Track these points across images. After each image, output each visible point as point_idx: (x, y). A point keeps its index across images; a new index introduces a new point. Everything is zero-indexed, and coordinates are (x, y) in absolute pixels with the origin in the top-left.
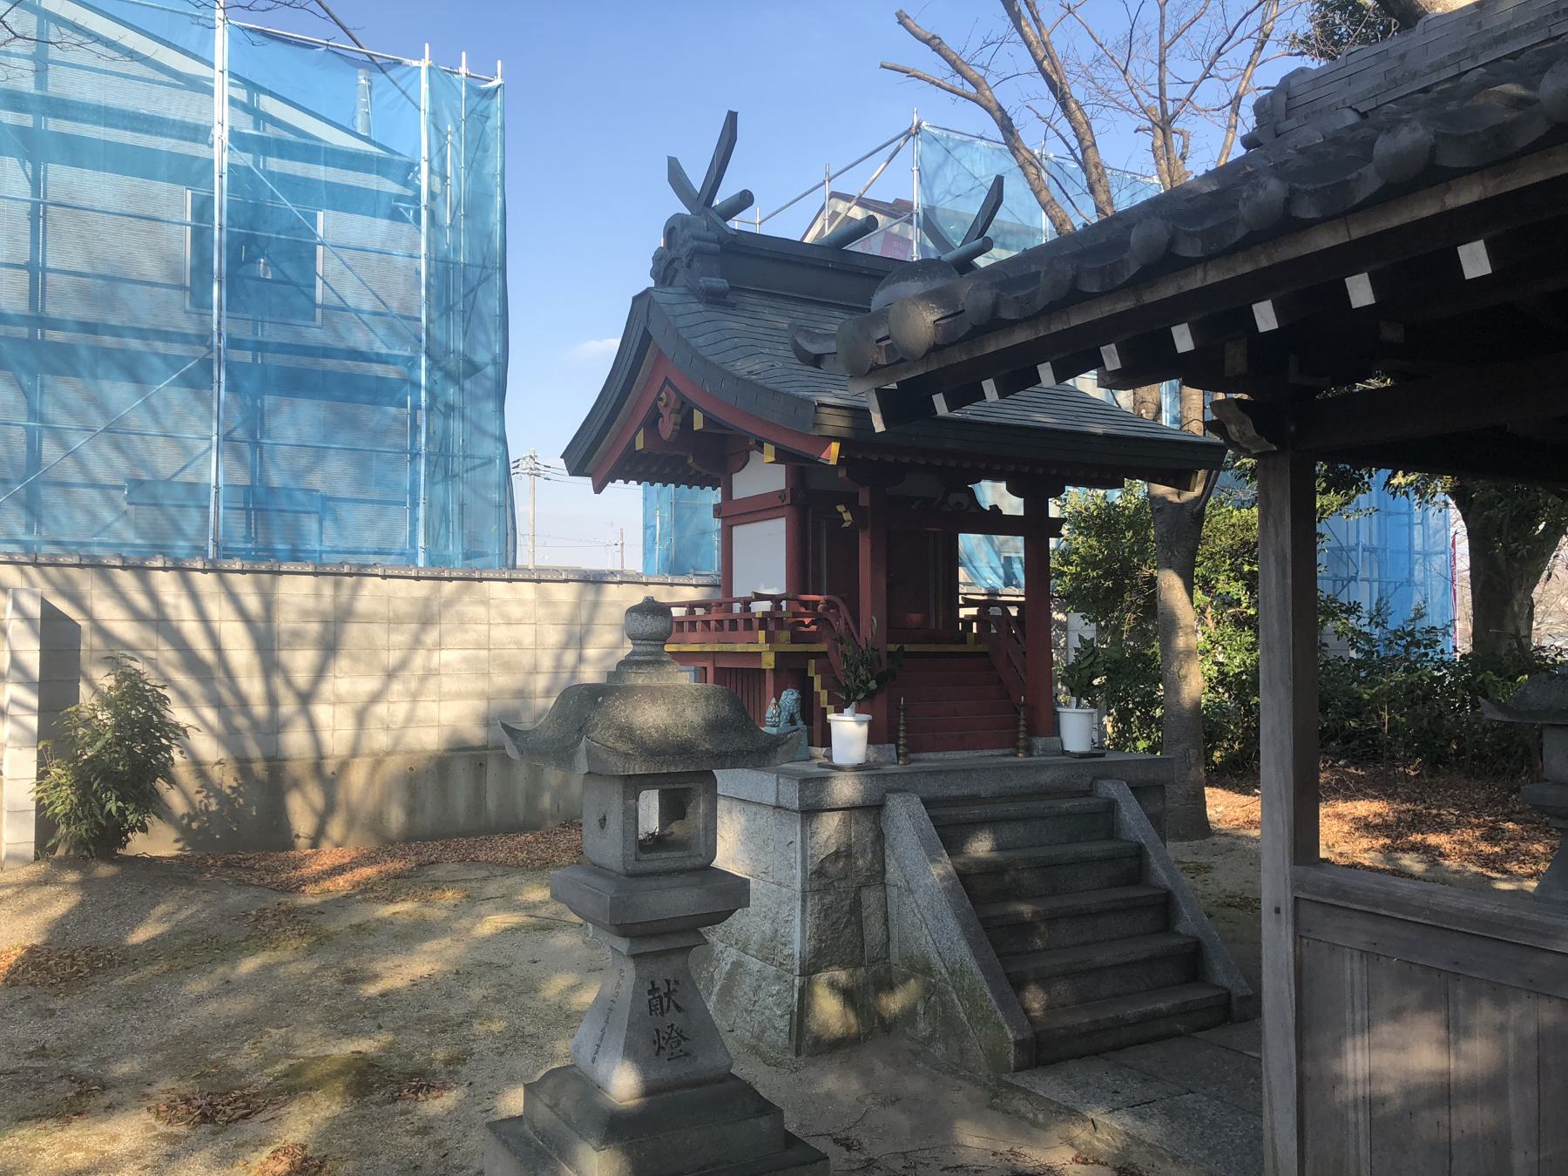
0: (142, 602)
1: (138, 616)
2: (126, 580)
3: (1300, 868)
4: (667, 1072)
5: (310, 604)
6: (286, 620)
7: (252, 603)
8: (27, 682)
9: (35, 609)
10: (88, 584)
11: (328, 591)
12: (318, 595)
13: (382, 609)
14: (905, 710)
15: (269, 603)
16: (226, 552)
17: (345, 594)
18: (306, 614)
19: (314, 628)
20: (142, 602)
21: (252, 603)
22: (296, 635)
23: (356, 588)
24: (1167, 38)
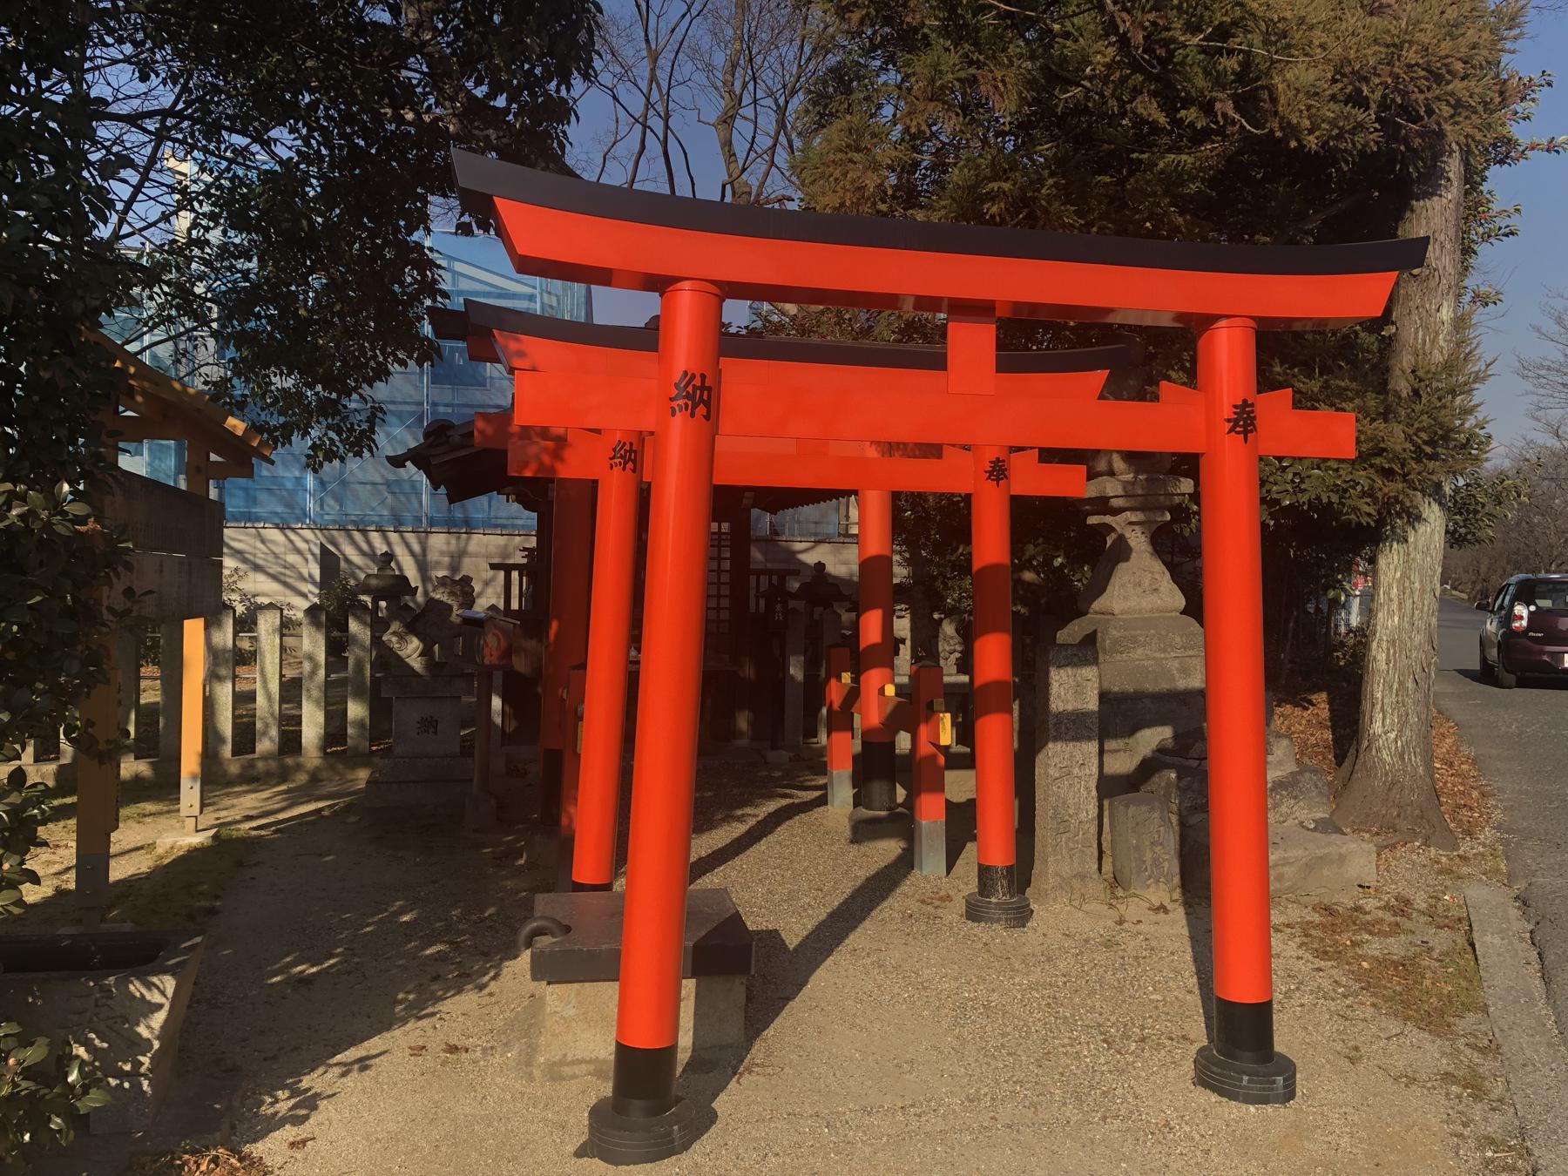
0: (365, 547)
1: (363, 553)
2: (358, 536)
3: (294, 712)
4: (1052, 721)
5: (445, 548)
6: (433, 556)
7: (416, 548)
8: (314, 582)
9: (317, 551)
10: (340, 538)
11: (453, 541)
12: (448, 543)
13: (483, 550)
14: (1536, 570)
15: (424, 550)
16: (432, 522)
17: (462, 543)
18: (442, 553)
19: (446, 560)
20: (365, 547)
21: (416, 548)
22: (438, 563)
23: (468, 540)
24: (782, 139)
